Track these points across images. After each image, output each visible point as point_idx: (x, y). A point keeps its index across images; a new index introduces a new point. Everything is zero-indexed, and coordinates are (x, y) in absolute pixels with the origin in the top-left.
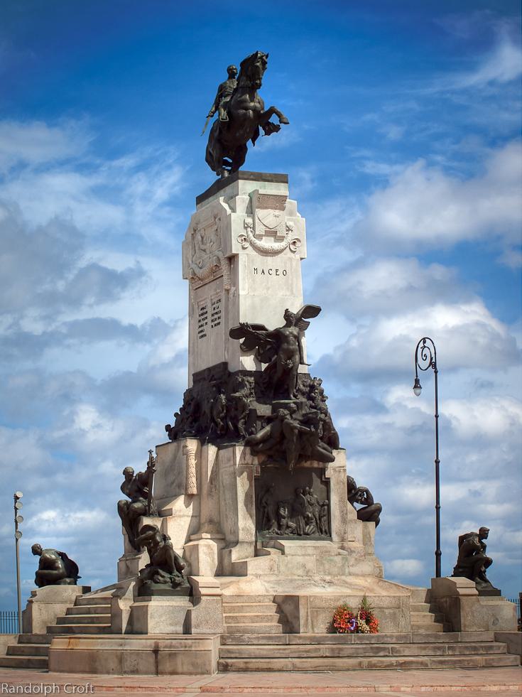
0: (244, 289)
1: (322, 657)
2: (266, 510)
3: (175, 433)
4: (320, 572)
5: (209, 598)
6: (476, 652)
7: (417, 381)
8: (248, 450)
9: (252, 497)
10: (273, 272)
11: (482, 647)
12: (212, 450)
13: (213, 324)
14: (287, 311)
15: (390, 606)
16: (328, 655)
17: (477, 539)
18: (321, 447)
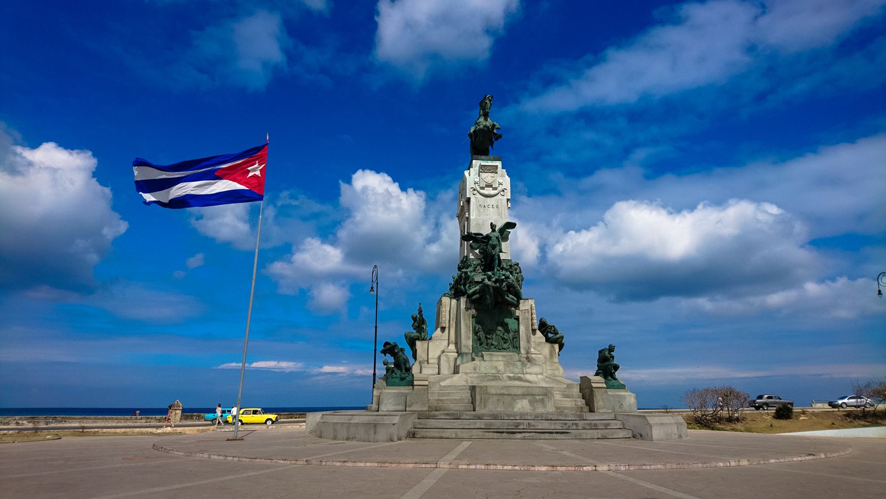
1: (478, 428)
4: (507, 371)
5: (419, 387)
6: (596, 428)
10: (491, 206)
11: (601, 424)
14: (491, 223)
16: (482, 427)
17: (607, 353)
18: (511, 298)
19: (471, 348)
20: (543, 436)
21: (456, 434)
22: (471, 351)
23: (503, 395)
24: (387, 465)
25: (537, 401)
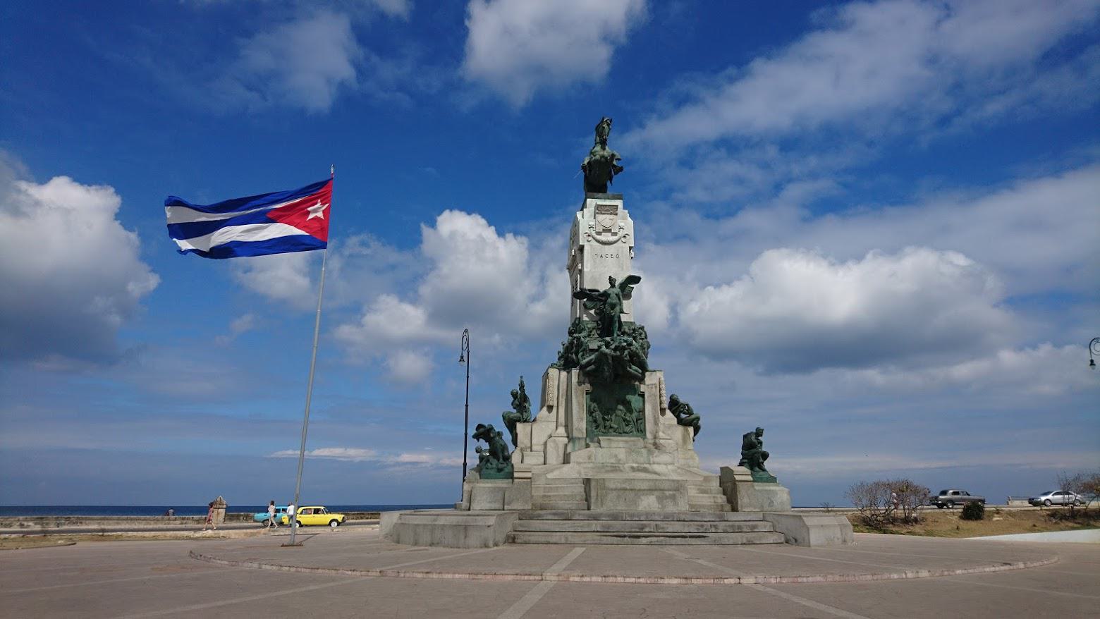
0: (587, 268)
7: (1092, 361)
14: (610, 277)
15: (670, 488)
16: (599, 530)
19: (585, 431)
20: (674, 541)
24: (480, 576)
25: (667, 498)
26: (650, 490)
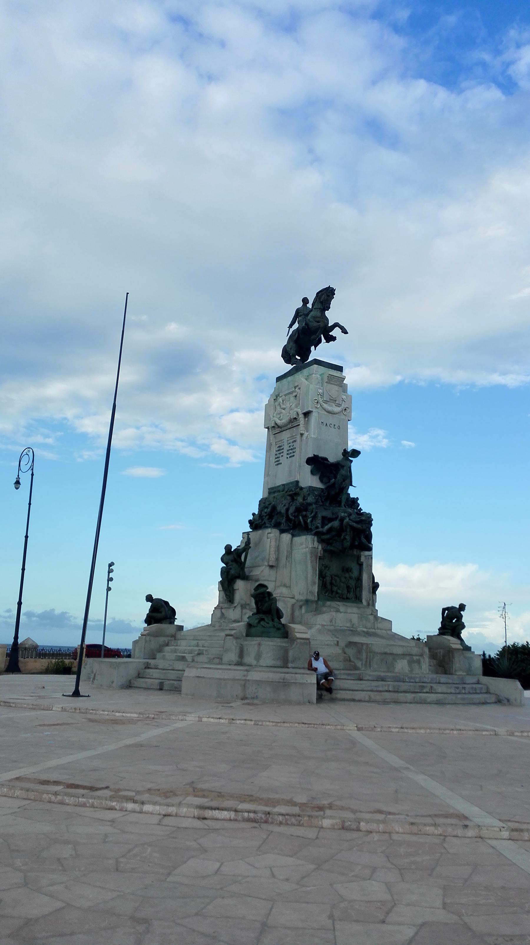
2: (325, 580)
3: (255, 524)
5: (301, 641)
8: (316, 538)
9: (316, 571)
12: (286, 537)
13: (288, 456)
19: (316, 595)
21: (370, 697)
22: (316, 599)
23: (386, 653)
24: (447, 731)
26: (403, 655)
